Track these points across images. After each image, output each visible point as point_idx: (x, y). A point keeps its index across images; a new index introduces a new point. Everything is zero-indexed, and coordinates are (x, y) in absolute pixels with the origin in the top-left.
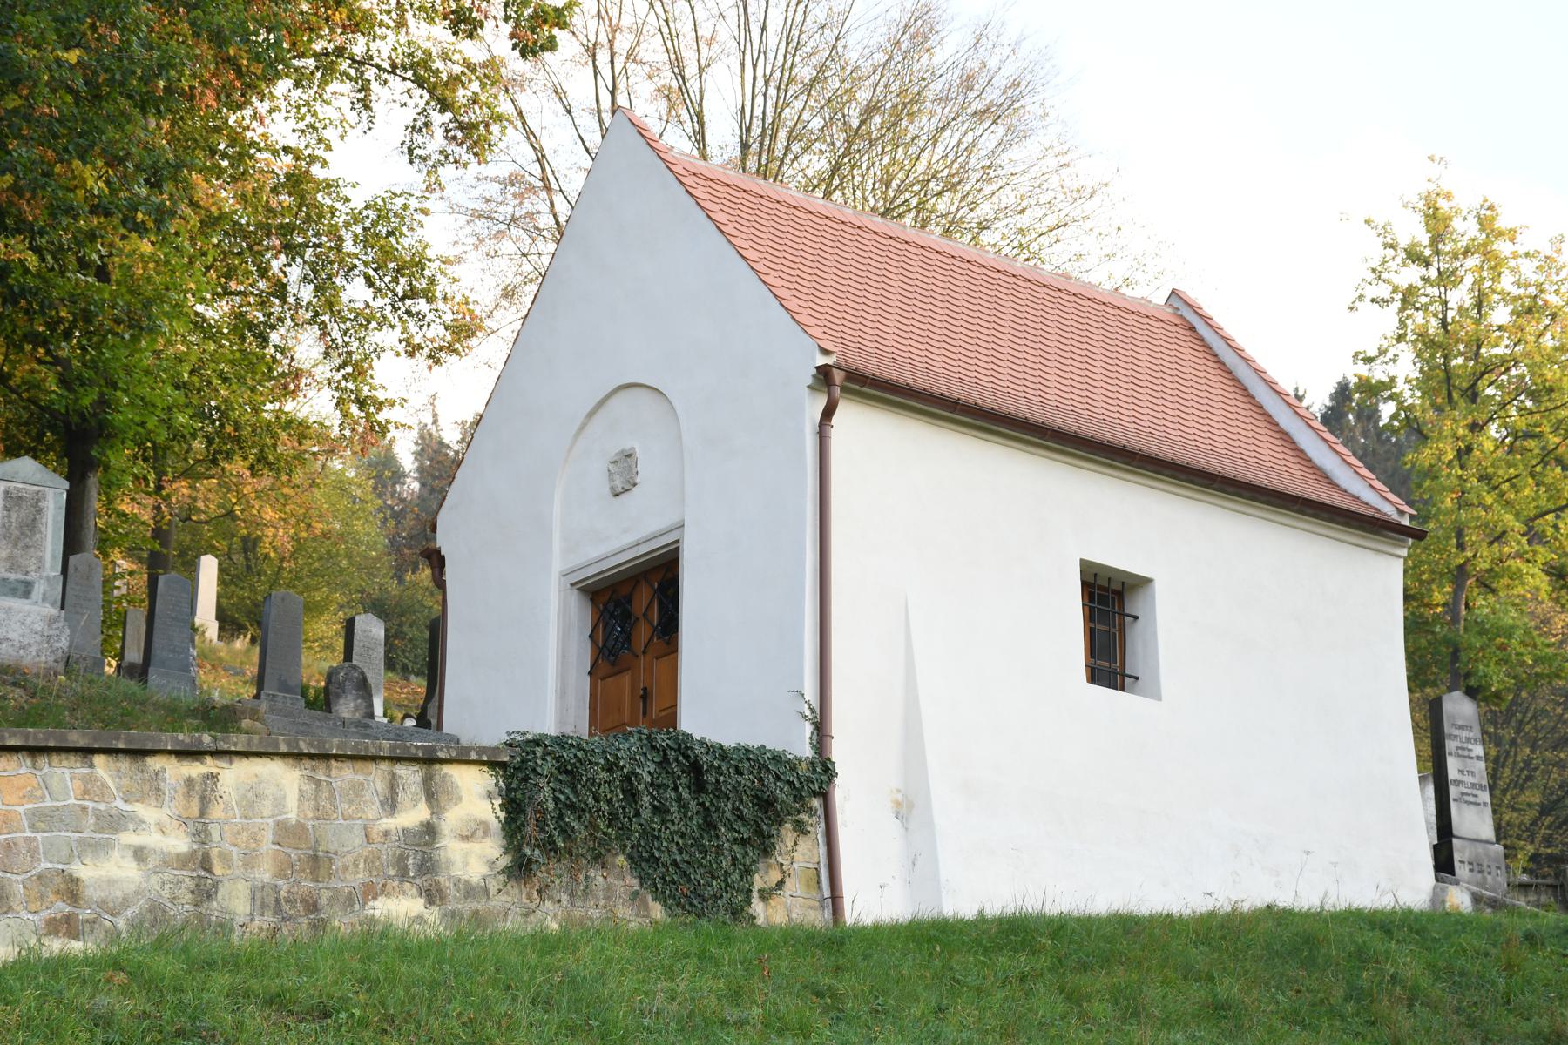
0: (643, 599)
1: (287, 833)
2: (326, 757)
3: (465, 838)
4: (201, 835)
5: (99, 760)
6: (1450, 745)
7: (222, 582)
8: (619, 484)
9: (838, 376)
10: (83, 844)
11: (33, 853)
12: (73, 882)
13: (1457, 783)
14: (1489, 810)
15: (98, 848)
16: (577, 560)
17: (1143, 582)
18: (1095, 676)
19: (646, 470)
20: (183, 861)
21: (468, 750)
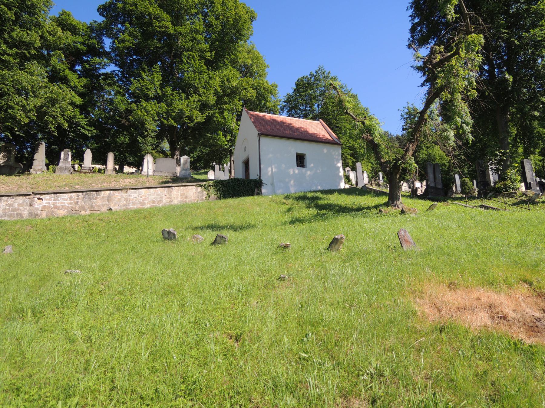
11: (148, 199)
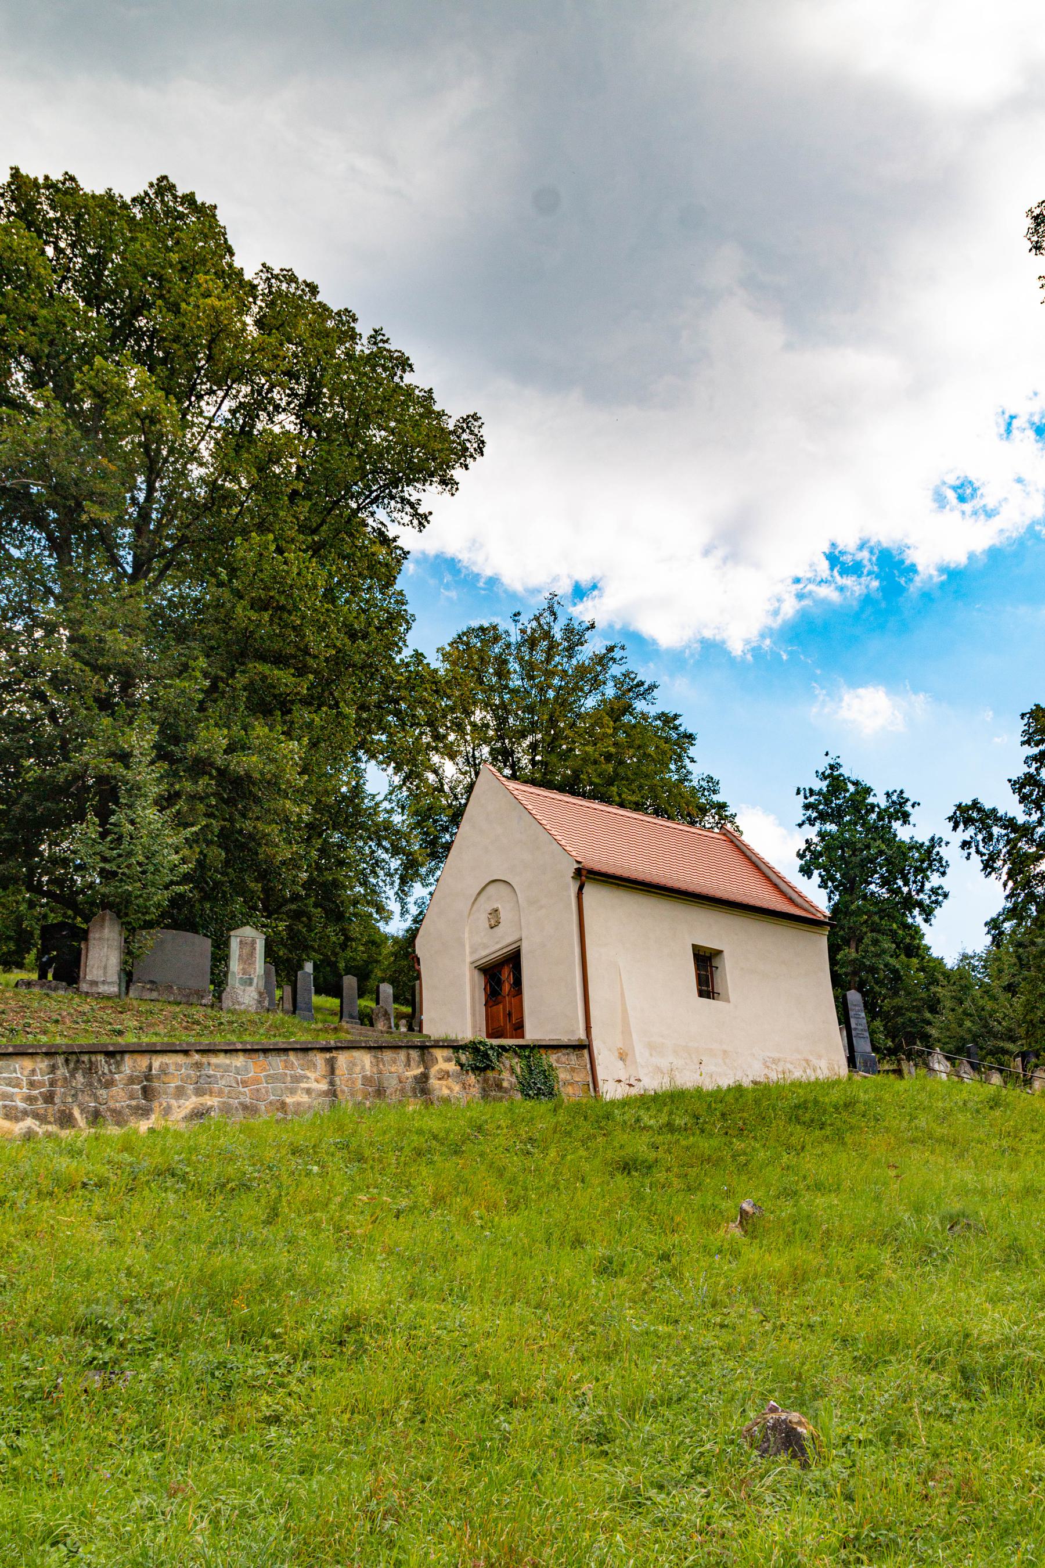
0: (506, 974)
1: (367, 1080)
2: (380, 1048)
3: (440, 1079)
4: (332, 1083)
5: (291, 1053)
6: (851, 1013)
7: (506, 1037)
8: (493, 923)
9: (584, 872)
10: (287, 1088)
12: (283, 1104)
13: (856, 1029)
14: (868, 1040)
15: (293, 1091)
16: (476, 956)
17: (719, 953)
18: (702, 994)
19: (503, 915)
20: (326, 1093)
21: (438, 1041)
